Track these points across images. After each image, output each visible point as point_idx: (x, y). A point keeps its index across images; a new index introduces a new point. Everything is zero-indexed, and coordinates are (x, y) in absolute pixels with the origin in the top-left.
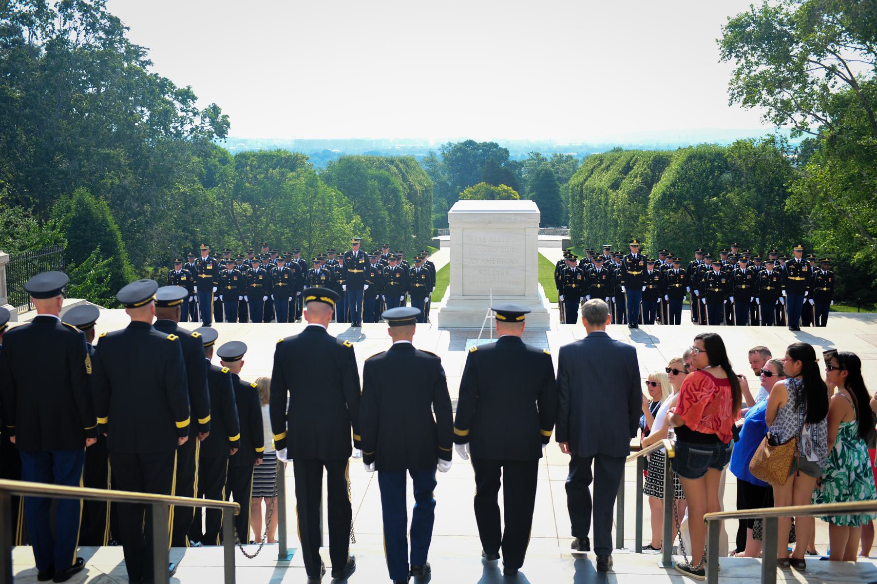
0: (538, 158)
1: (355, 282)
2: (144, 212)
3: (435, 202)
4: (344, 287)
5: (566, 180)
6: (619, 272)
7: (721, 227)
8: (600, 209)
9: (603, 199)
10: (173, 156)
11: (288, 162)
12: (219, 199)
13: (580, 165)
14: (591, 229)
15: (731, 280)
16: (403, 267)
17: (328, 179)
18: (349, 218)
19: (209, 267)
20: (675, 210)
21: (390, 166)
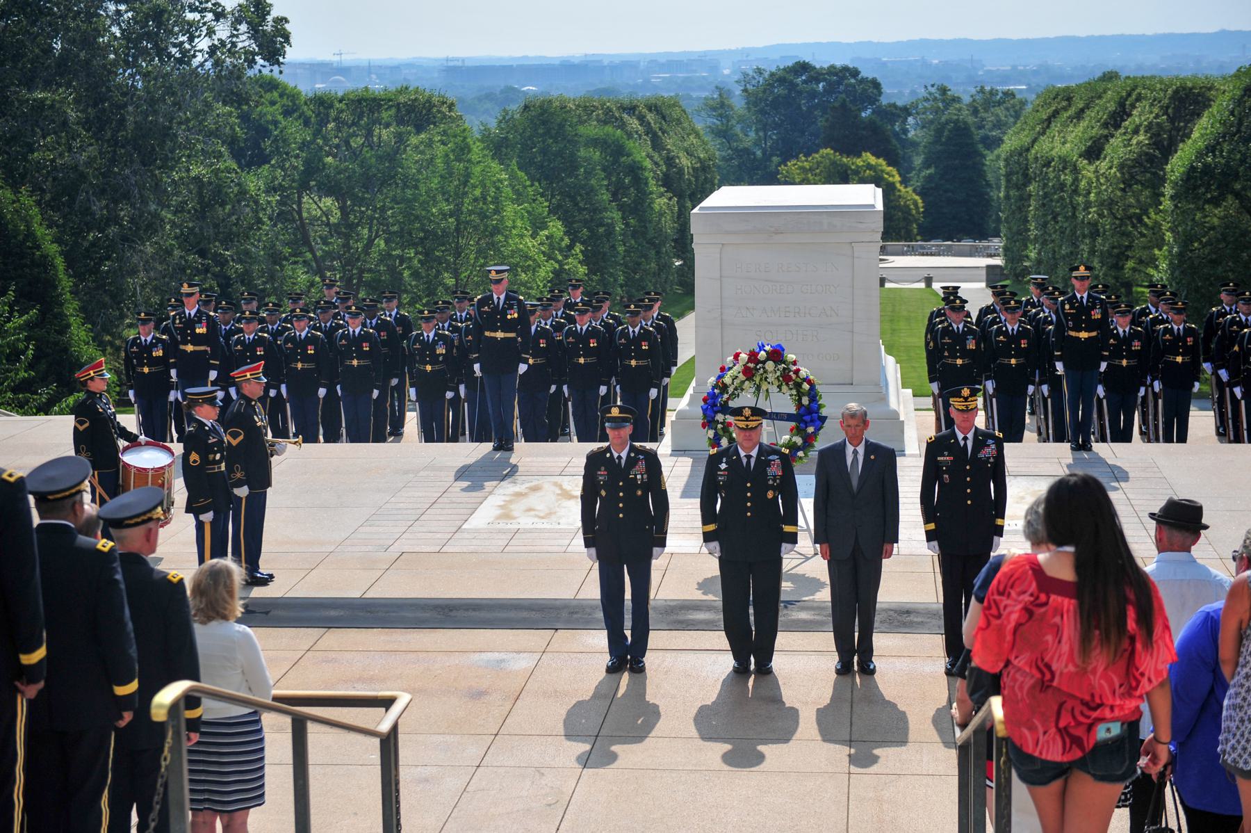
2: (117, 221)
5: (998, 142)
8: (1060, 202)
10: (174, 104)
11: (417, 111)
14: (1044, 243)
18: (538, 225)
19: (201, 330)
20: (1216, 202)
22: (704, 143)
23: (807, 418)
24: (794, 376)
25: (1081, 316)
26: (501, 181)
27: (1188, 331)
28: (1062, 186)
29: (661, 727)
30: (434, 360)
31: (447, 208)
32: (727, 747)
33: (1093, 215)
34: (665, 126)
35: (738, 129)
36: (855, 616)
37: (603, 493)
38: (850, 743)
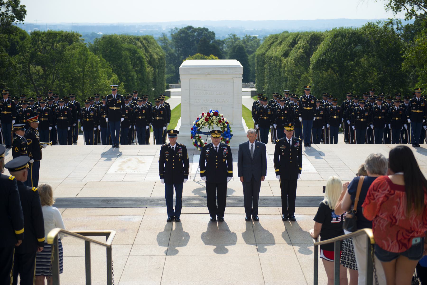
0: (235, 38)
1: (115, 116)
3: (166, 67)
4: (107, 119)
6: (296, 108)
7: (356, 80)
9: (278, 63)
11: (69, 38)
12: (20, 63)
13: (262, 43)
14: (270, 83)
15: (372, 113)
16: (148, 105)
17: (95, 50)
18: (110, 76)
20: (326, 70)
21: (137, 42)
22: (161, 50)
23: (227, 135)
24: (222, 121)
25: (307, 102)
26: (98, 61)
27: (338, 108)
28: (276, 66)
29: (191, 241)
30: (90, 117)
31: (80, 70)
32: (215, 247)
33: (286, 74)
34: (149, 45)
35: (170, 47)
36: (251, 202)
37: (167, 160)
38: (256, 244)
